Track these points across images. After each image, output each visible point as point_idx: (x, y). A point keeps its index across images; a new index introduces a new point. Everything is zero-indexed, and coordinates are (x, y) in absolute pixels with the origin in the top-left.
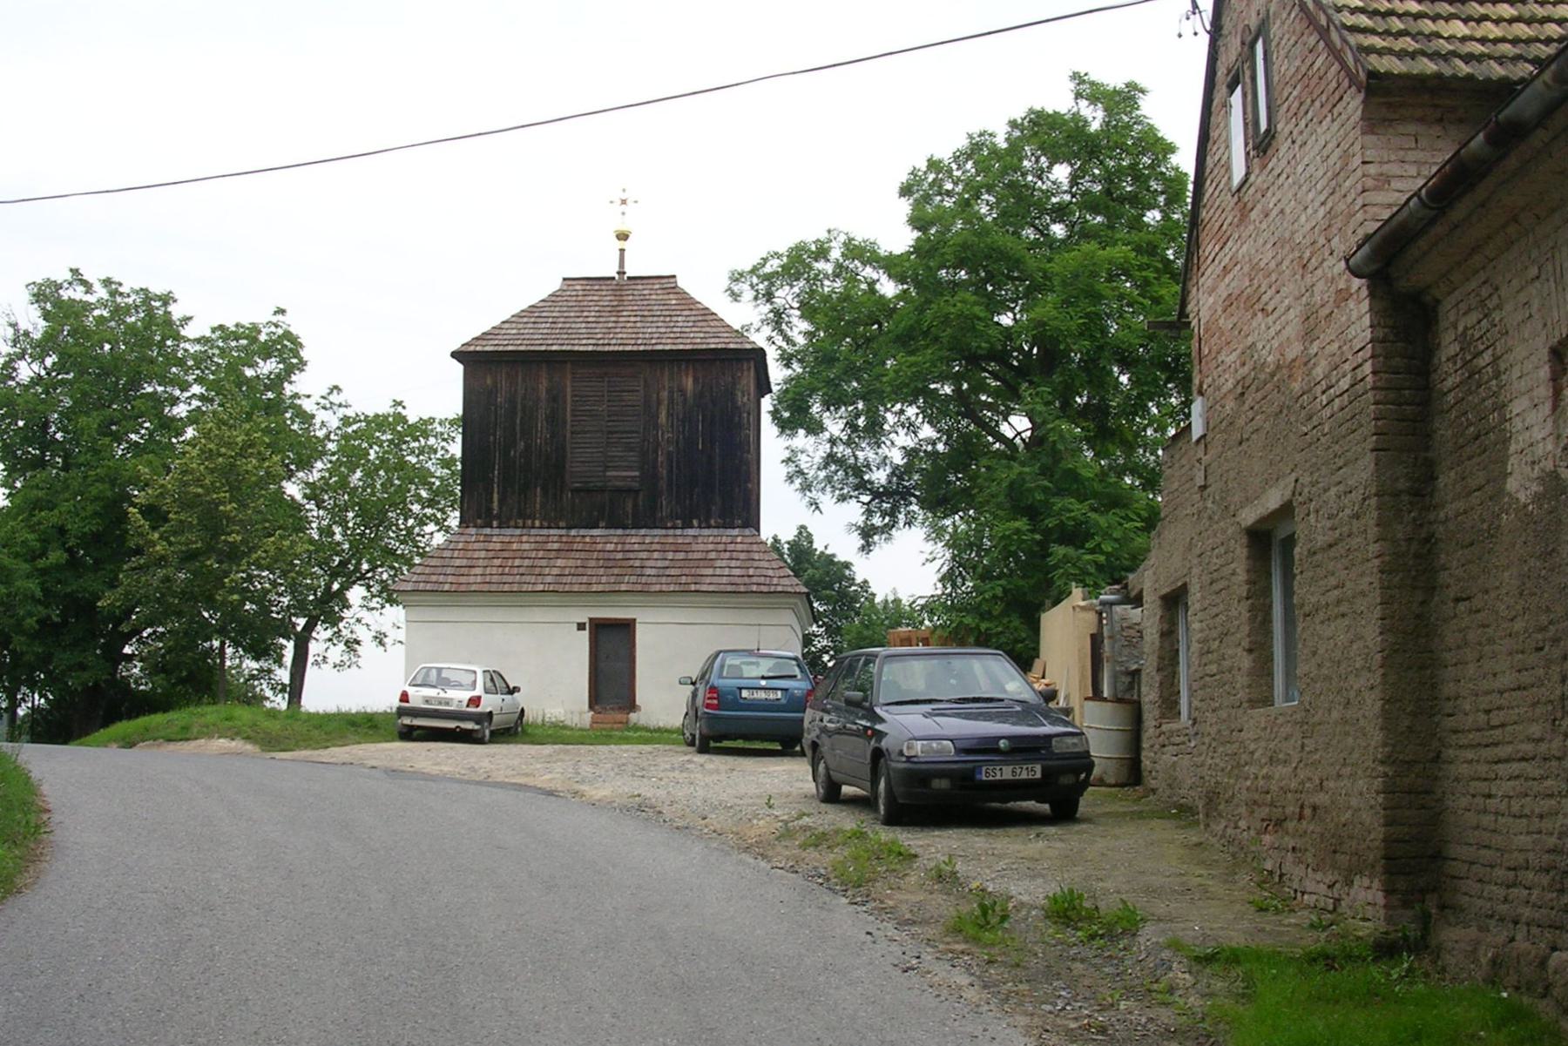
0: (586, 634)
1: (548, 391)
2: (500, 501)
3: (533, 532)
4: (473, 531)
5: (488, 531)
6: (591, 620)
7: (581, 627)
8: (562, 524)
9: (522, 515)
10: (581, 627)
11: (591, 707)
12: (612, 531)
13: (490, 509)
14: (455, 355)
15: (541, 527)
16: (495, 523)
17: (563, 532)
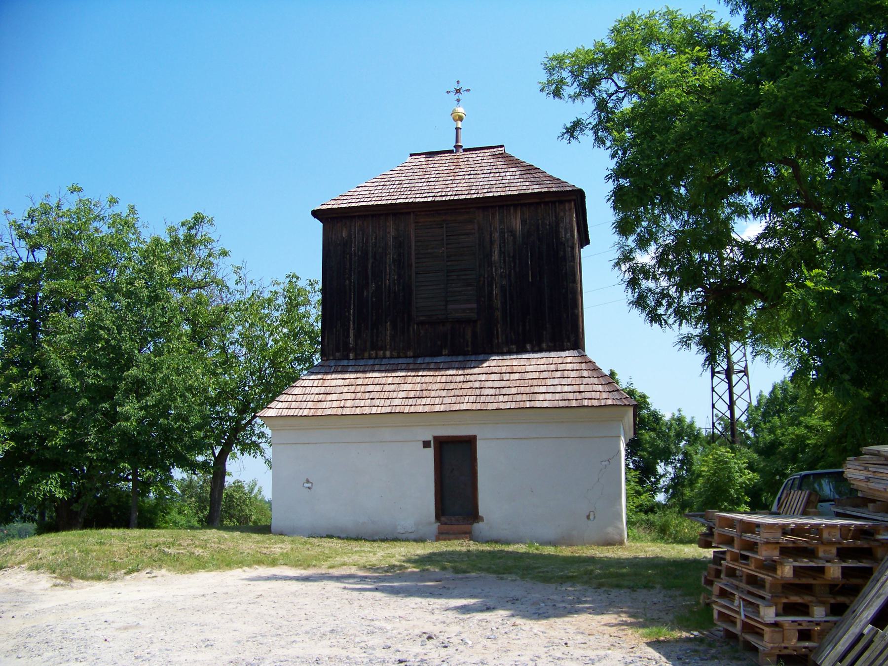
0: (430, 452)
1: (394, 238)
2: (355, 336)
3: (384, 361)
4: (332, 363)
5: (345, 362)
6: (435, 438)
7: (426, 444)
8: (410, 353)
9: (374, 347)
10: (426, 444)
11: (438, 517)
12: (454, 358)
13: (346, 344)
14: (316, 214)
15: (391, 357)
16: (351, 356)
17: (411, 360)
